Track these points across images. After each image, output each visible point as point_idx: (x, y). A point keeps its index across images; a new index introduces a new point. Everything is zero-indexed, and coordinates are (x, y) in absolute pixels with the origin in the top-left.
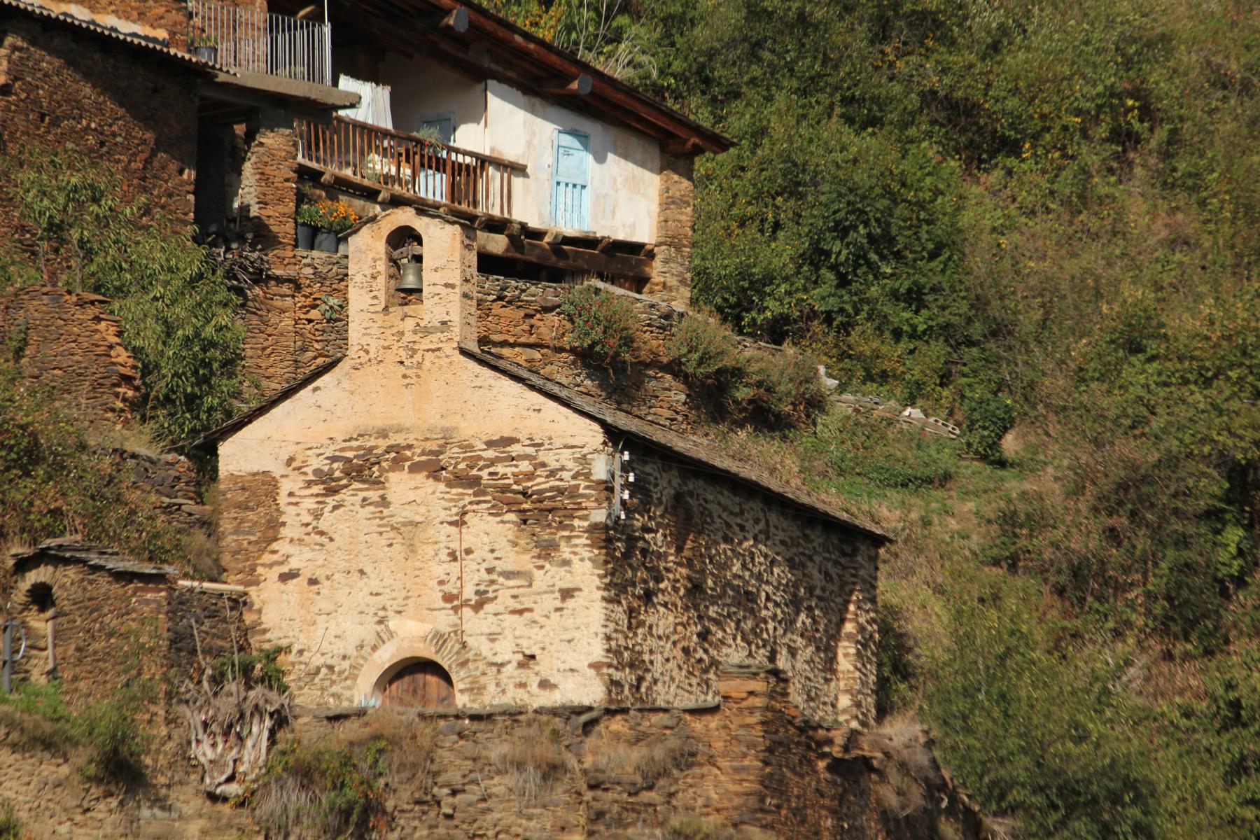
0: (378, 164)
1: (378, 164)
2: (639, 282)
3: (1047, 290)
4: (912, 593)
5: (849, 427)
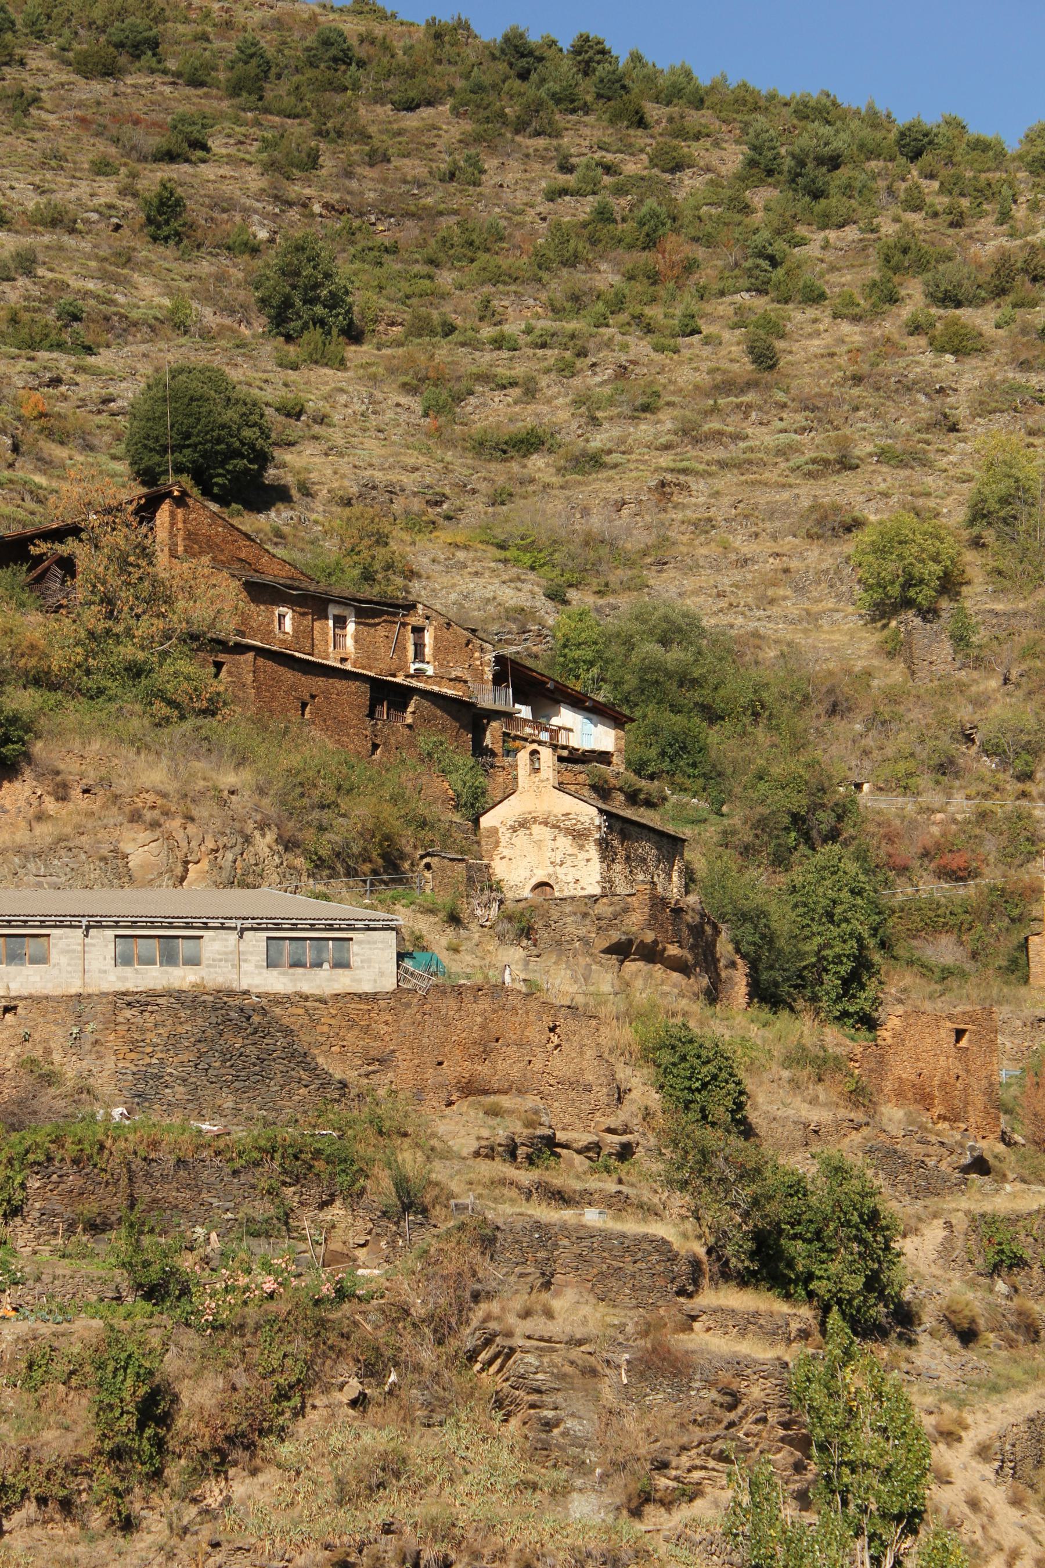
0: (528, 730)
1: (528, 730)
2: (609, 764)
3: (734, 762)
4: (695, 857)
5: (675, 806)
